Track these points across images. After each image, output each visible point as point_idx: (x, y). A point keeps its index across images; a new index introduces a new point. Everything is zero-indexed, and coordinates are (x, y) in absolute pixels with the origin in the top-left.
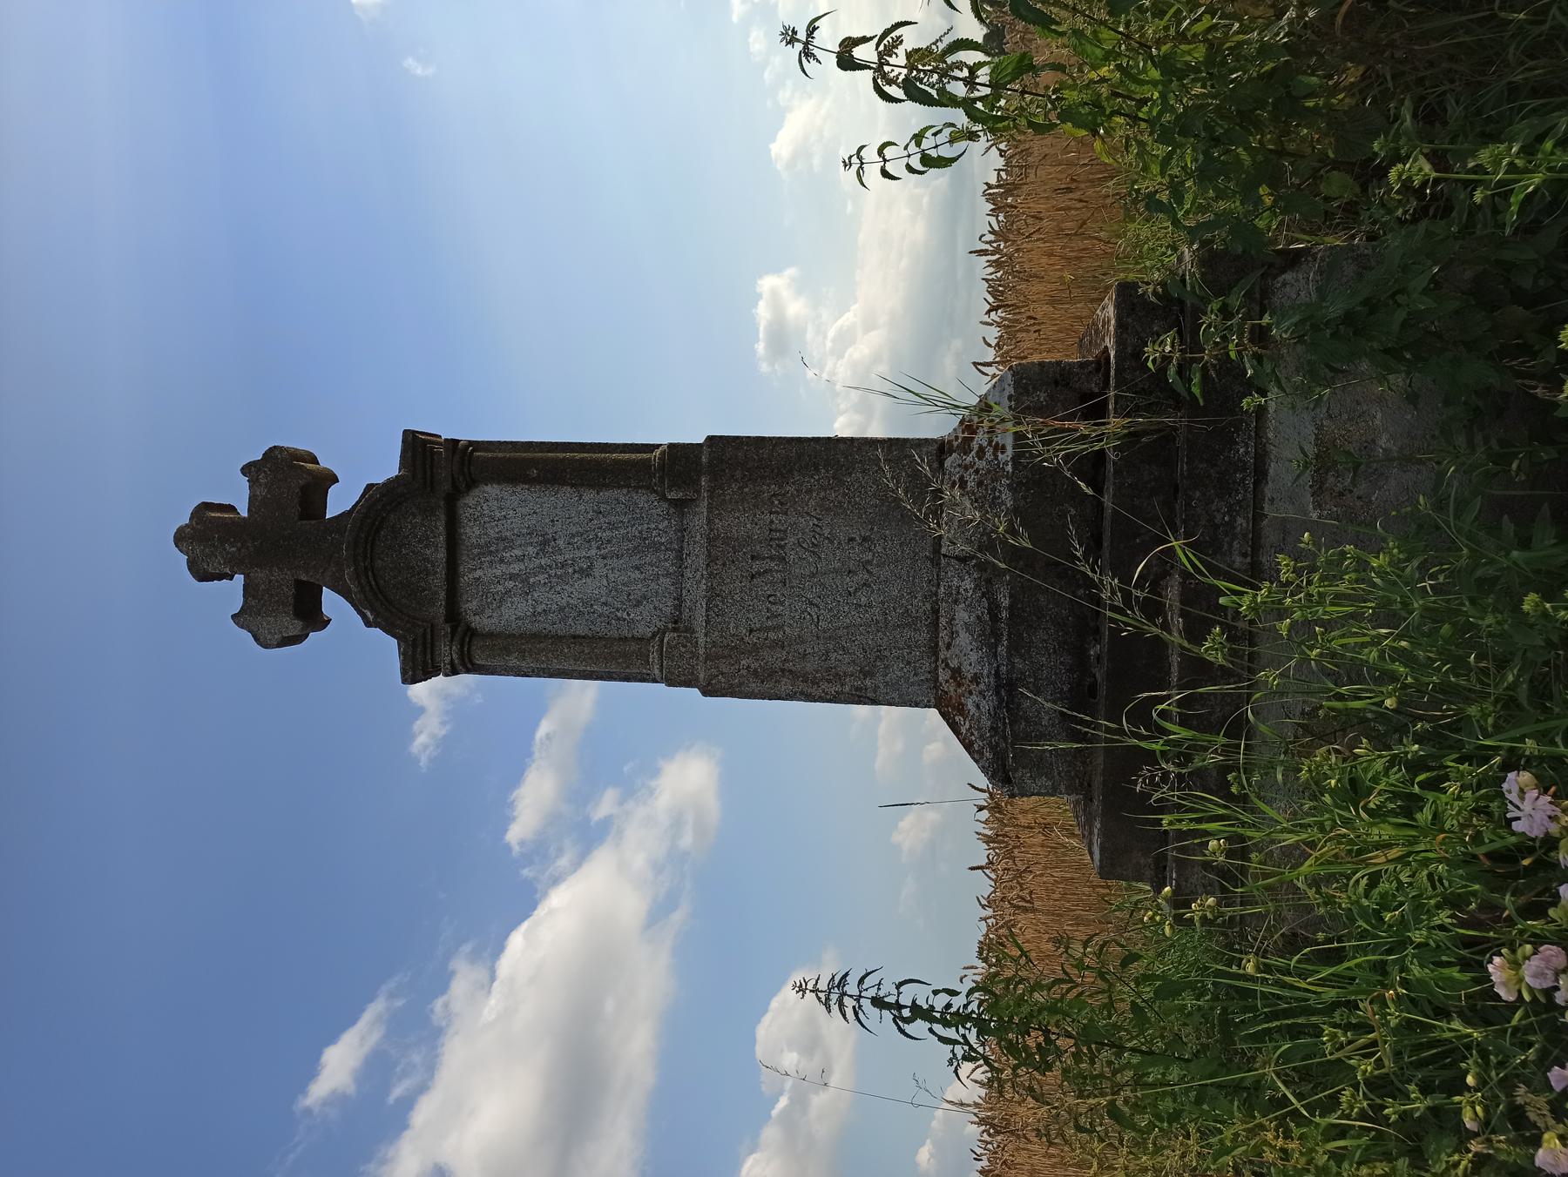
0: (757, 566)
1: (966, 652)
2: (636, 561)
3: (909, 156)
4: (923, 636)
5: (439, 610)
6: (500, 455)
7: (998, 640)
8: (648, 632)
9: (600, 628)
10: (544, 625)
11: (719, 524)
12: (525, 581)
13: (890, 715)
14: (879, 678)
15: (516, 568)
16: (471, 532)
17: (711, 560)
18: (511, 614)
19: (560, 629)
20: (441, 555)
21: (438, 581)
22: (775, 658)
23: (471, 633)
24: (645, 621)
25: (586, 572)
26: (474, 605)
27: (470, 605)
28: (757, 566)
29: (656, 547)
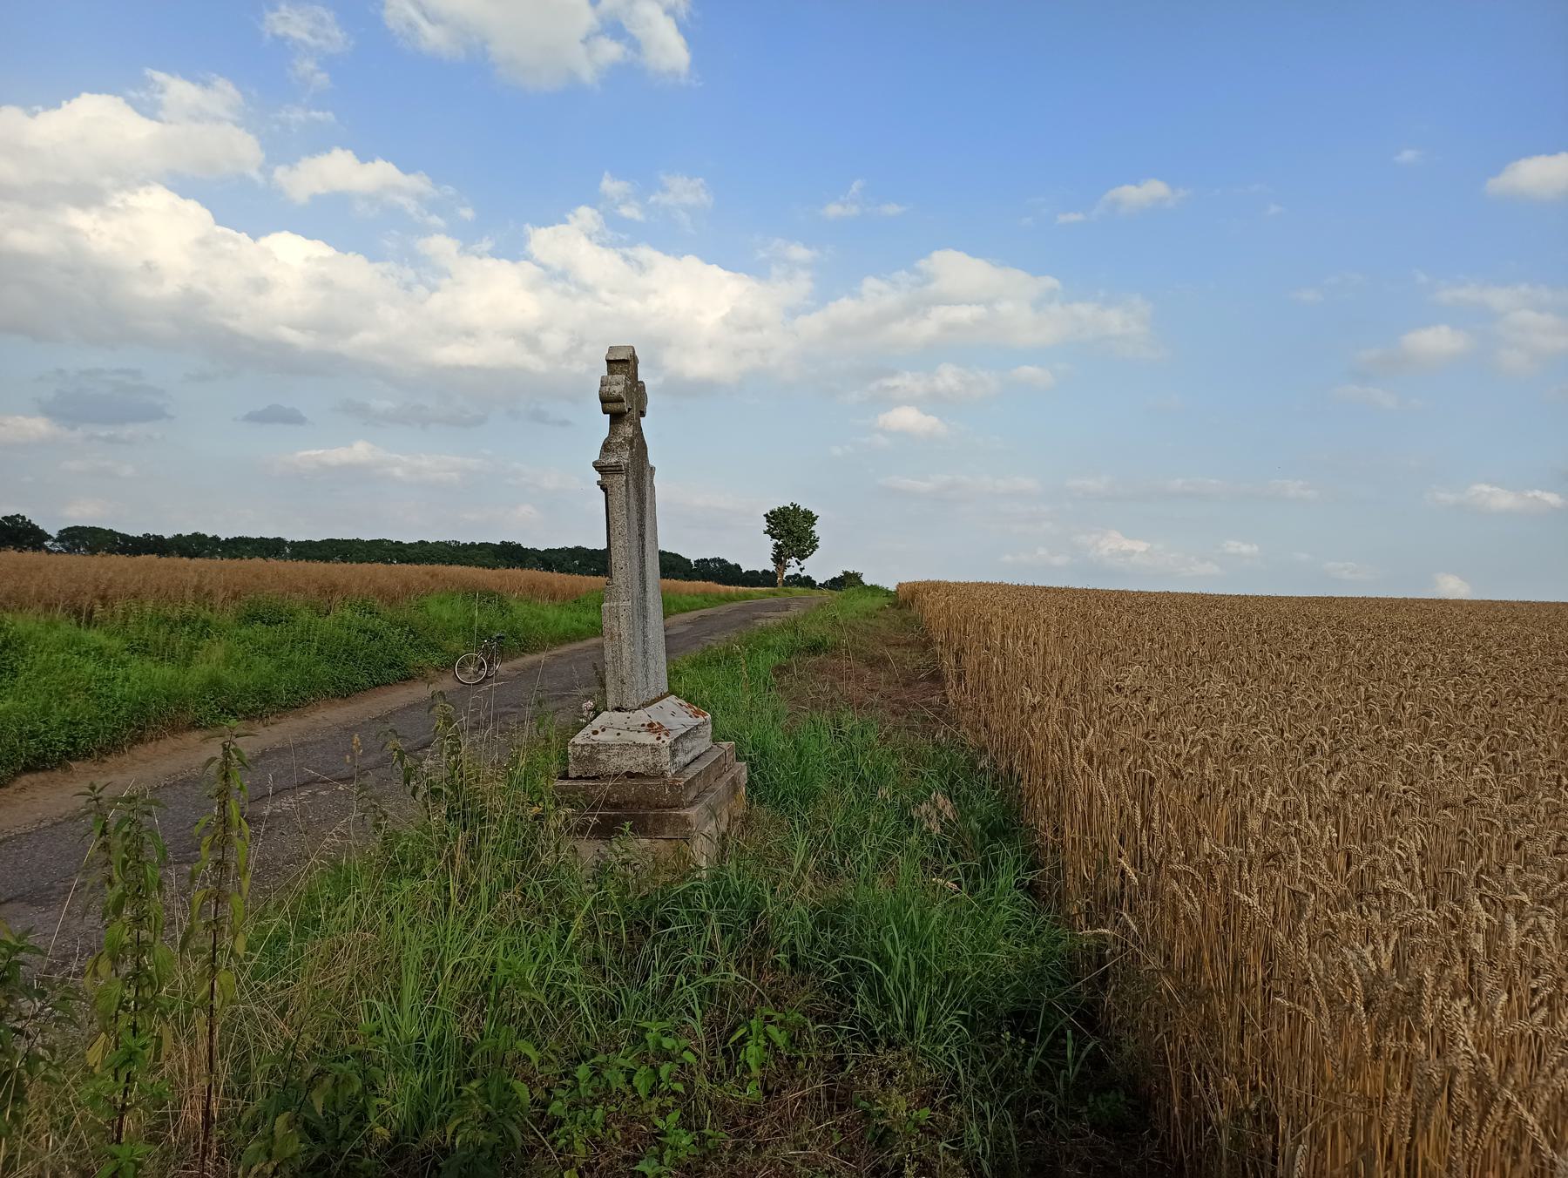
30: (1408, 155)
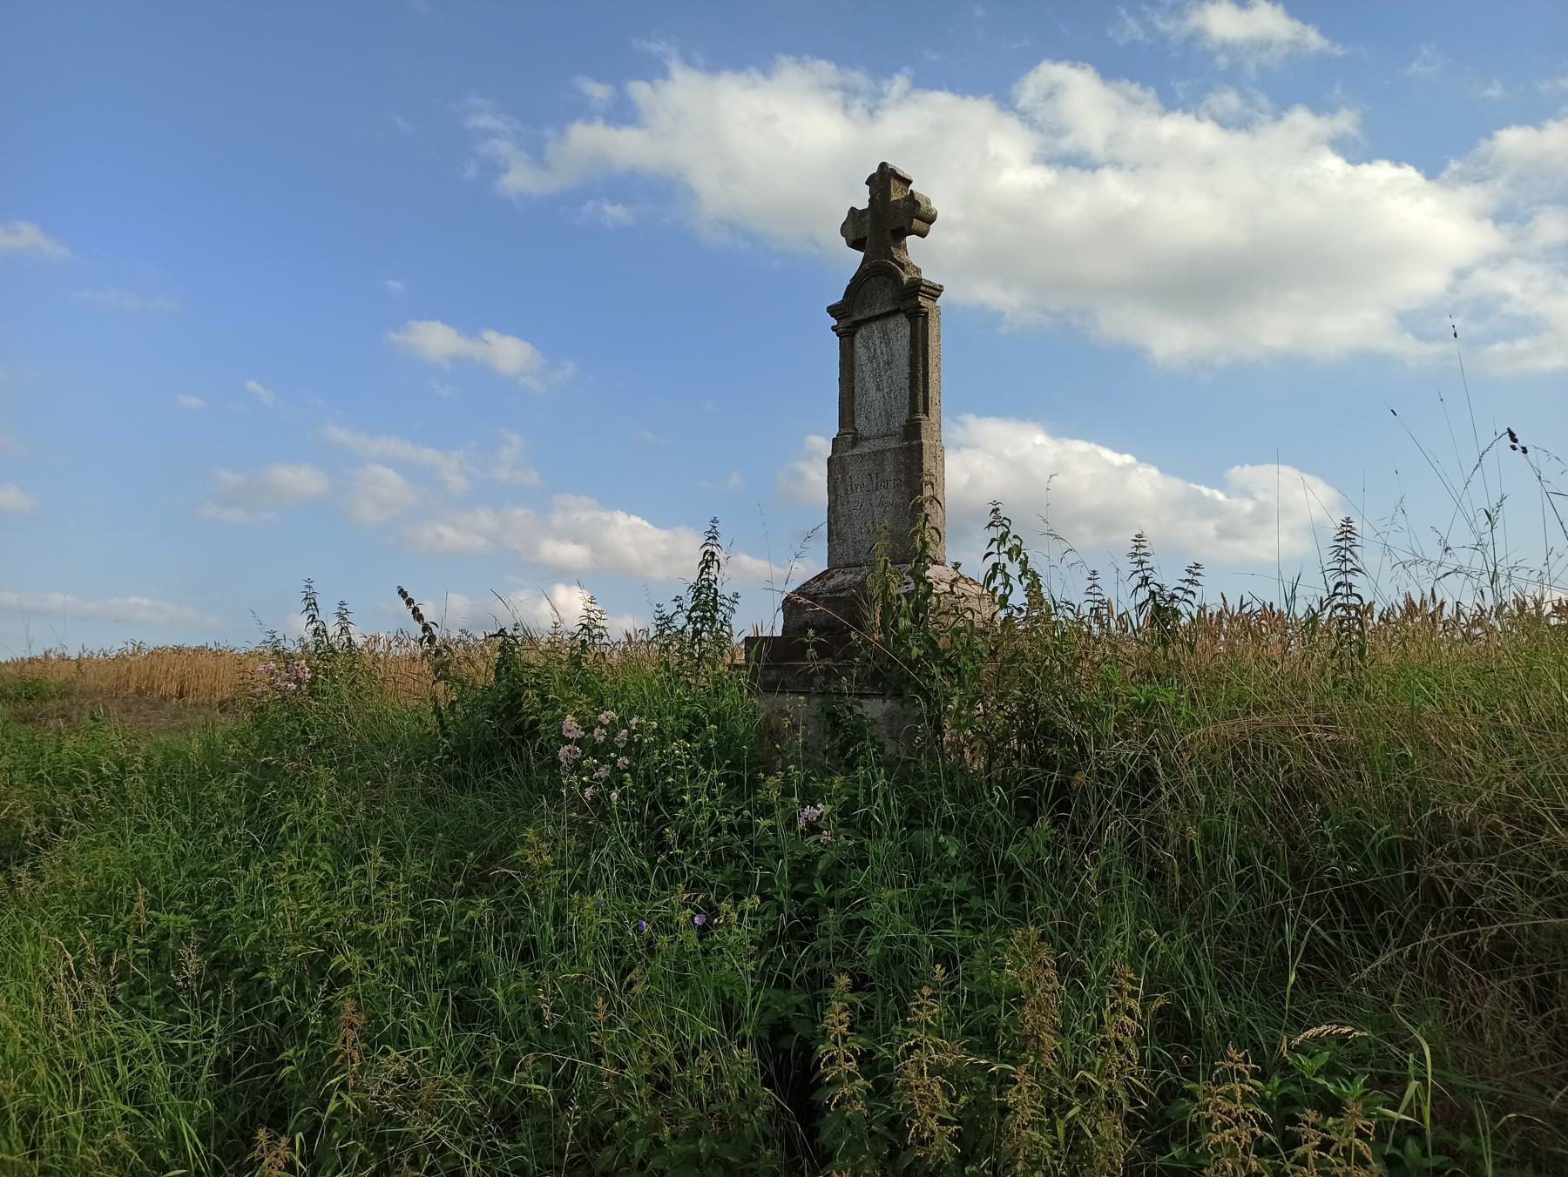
0: (874, 476)
1: (839, 578)
2: (883, 413)
3: (999, 554)
4: (852, 561)
5: (858, 317)
6: (920, 332)
7: (831, 593)
8: (857, 426)
9: (857, 400)
10: (857, 372)
11: (888, 455)
12: (874, 357)
13: (1267, 467)
14: (836, 541)
15: (878, 351)
16: (891, 323)
17: (875, 453)
18: (861, 354)
19: (856, 380)
20: (877, 312)
21: (867, 313)
22: (841, 492)
23: (853, 335)
24: (861, 423)
25: (878, 389)
26: (864, 333)
27: (863, 331)
28: (874, 476)
29: (888, 424)
30: (395, 285)
